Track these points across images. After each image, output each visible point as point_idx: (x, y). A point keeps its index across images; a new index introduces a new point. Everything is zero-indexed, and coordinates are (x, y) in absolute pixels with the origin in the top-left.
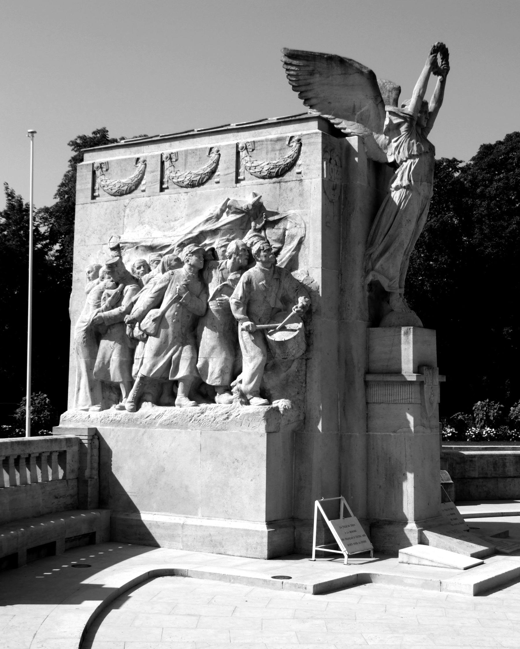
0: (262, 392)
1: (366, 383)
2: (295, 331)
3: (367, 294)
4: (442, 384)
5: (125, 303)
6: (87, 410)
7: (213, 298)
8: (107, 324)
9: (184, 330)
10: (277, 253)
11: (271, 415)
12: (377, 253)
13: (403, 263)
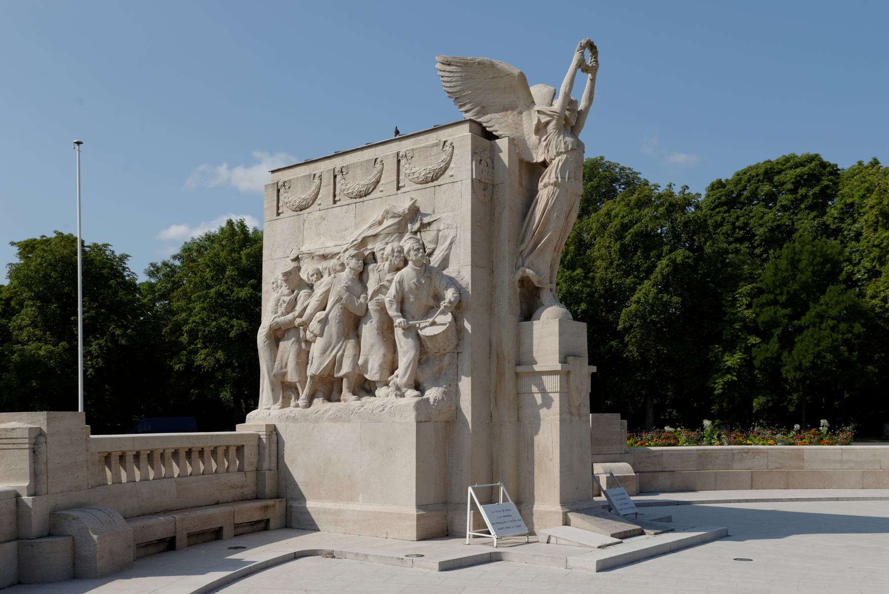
0: (418, 386)
1: (517, 375)
2: (445, 324)
3: (518, 290)
4: (593, 375)
5: (298, 308)
6: (269, 409)
7: (371, 299)
8: (283, 329)
9: (346, 330)
10: (430, 255)
11: (422, 406)
12: (527, 251)
13: (553, 259)
